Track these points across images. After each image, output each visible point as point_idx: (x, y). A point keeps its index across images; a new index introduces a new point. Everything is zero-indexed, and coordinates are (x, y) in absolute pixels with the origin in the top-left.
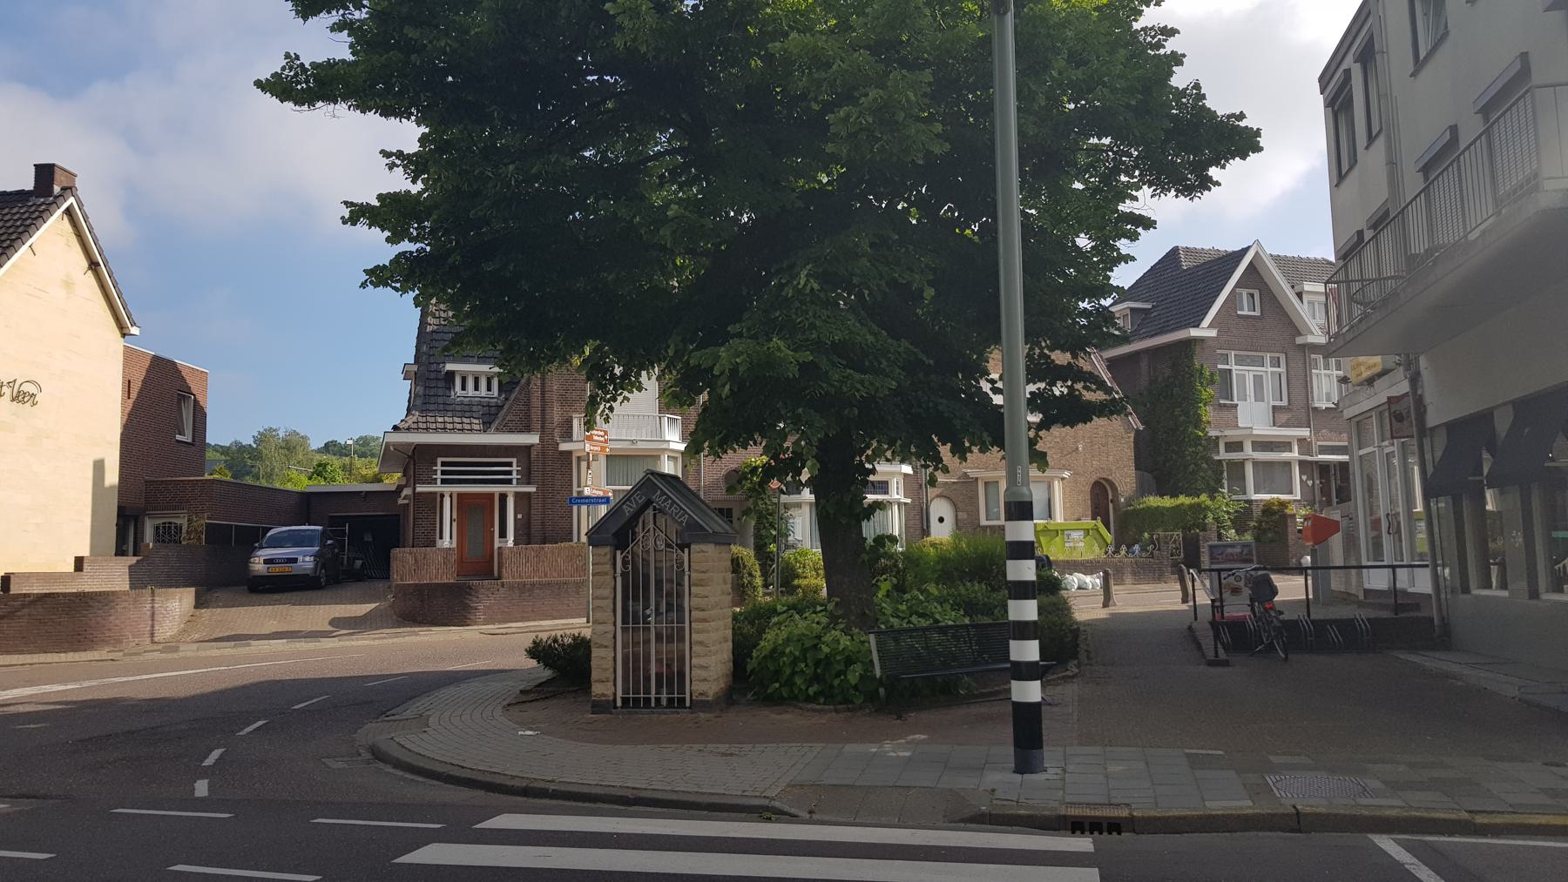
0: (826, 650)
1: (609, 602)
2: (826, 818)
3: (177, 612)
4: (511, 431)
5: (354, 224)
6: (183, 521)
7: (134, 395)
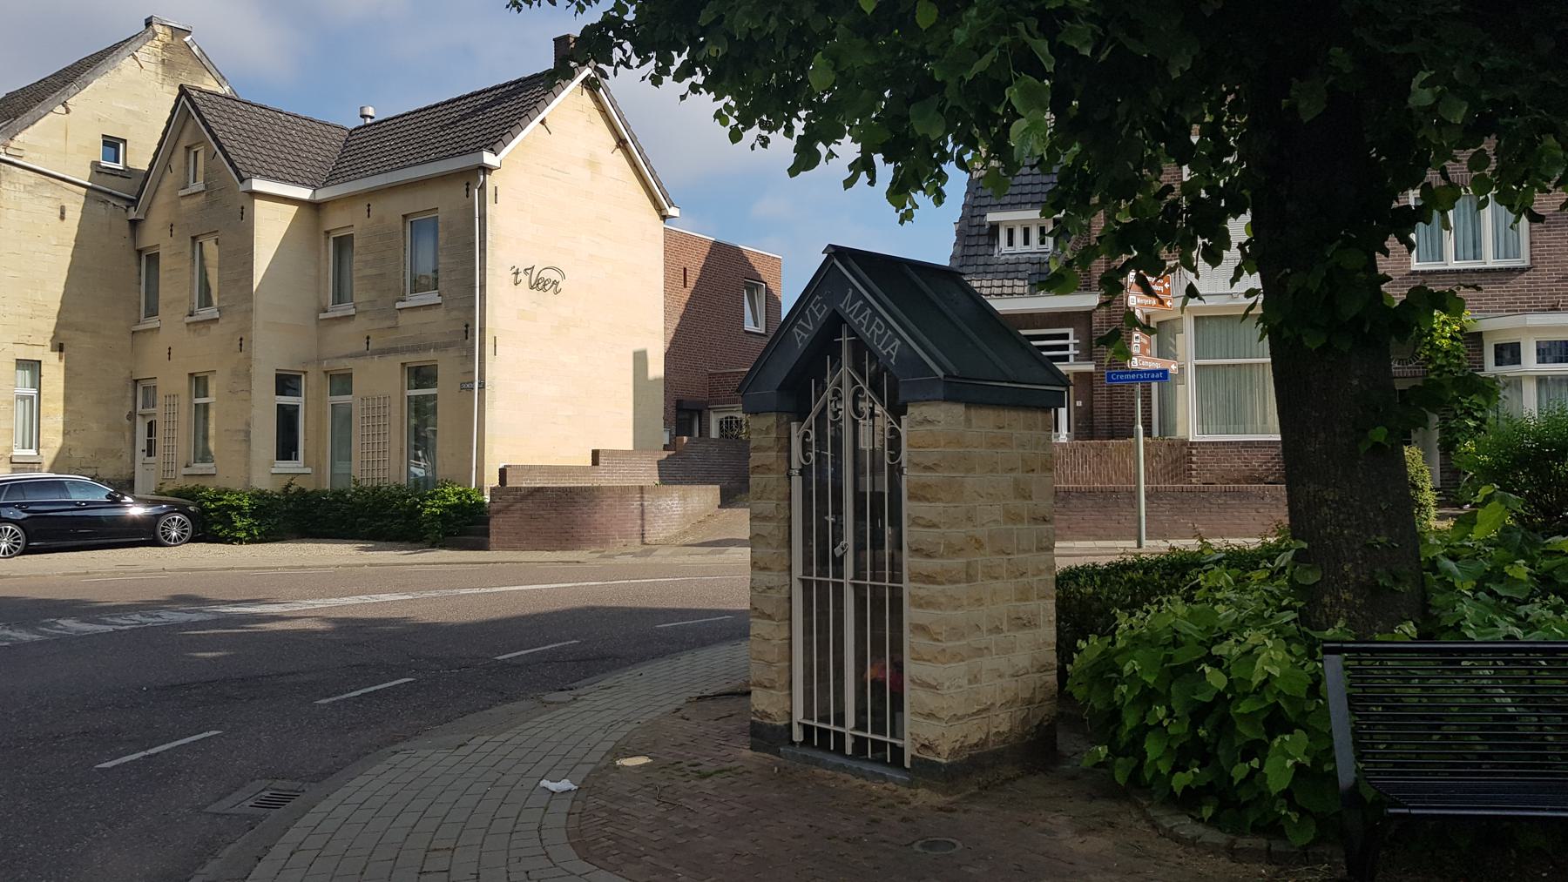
0: (1216, 679)
7: (691, 284)
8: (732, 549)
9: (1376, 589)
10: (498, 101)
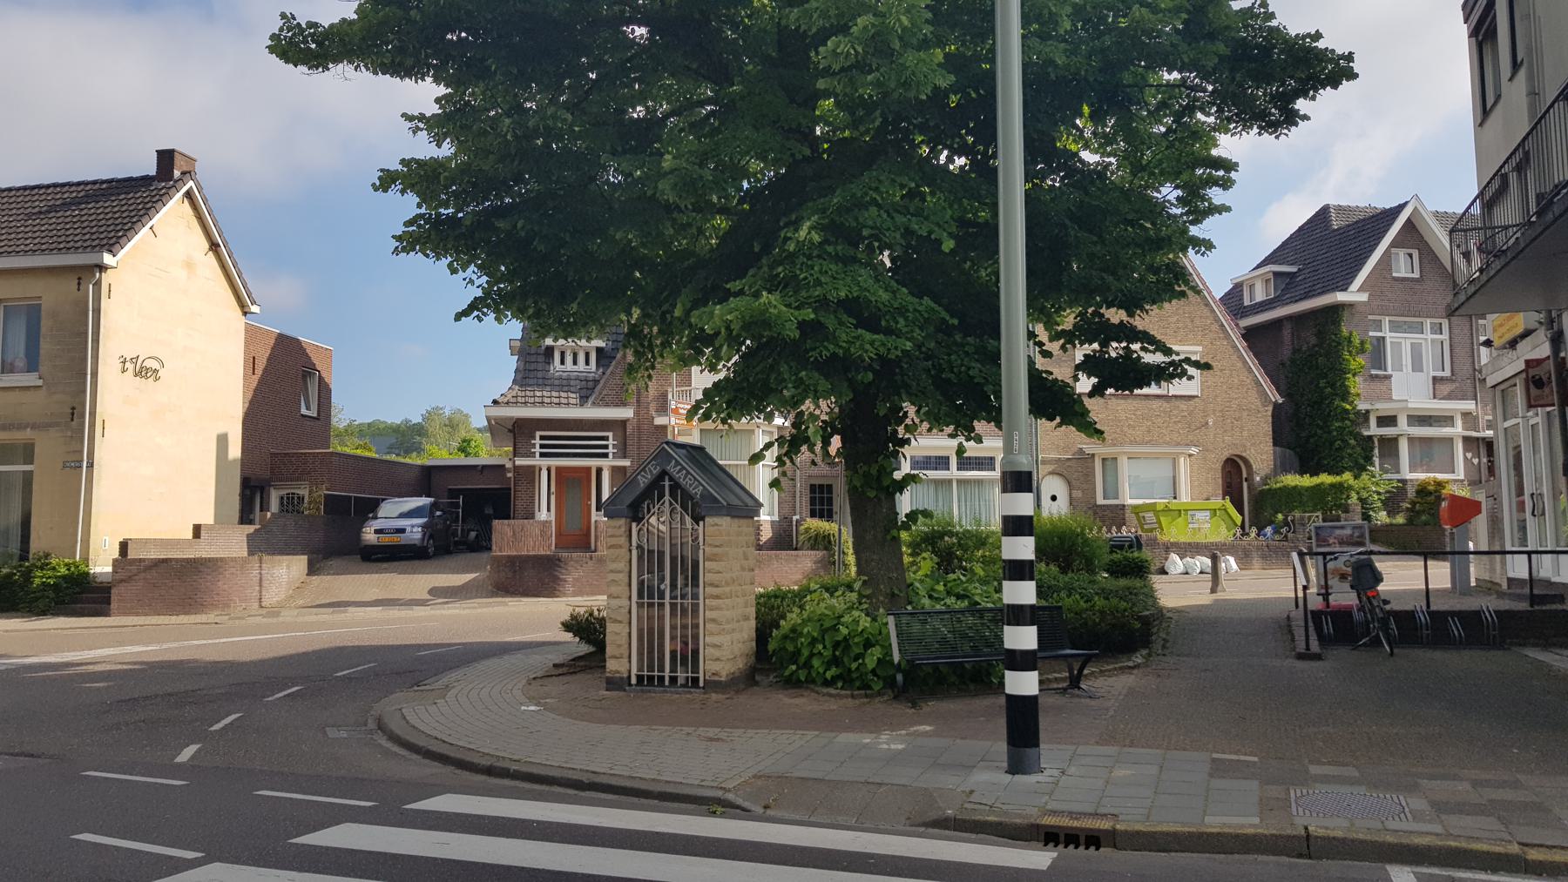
0: (844, 631)
1: (623, 577)
2: (786, 815)
4: (607, 405)
5: (385, 191)
7: (259, 372)
8: (350, 609)
9: (893, 595)
10: (88, 198)
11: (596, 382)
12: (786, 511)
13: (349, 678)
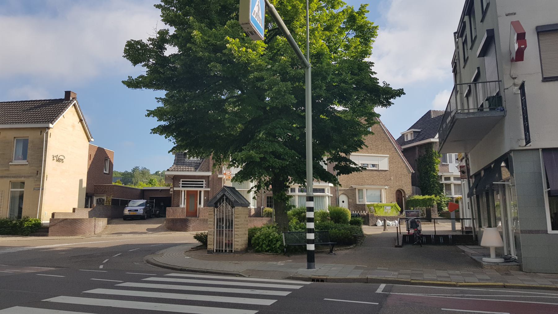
0: (271, 237)
3: (102, 225)
4: (203, 171)
6: (105, 198)
10: (43, 105)
11: (200, 164)
12: (259, 205)
13: (133, 251)
